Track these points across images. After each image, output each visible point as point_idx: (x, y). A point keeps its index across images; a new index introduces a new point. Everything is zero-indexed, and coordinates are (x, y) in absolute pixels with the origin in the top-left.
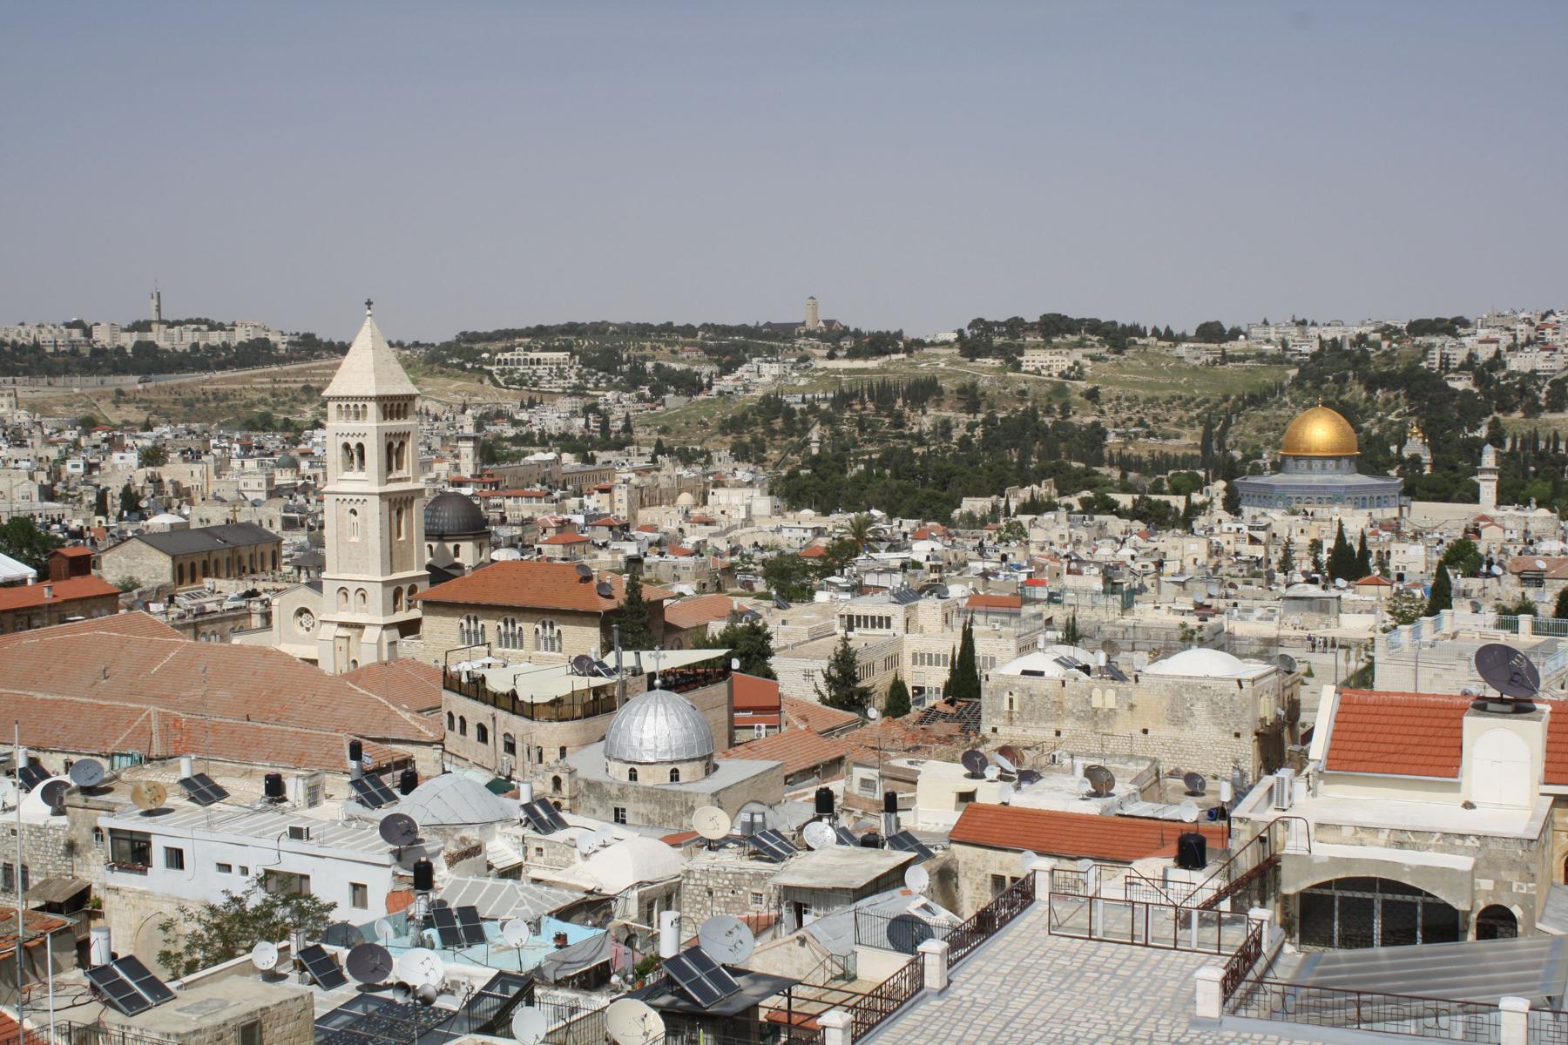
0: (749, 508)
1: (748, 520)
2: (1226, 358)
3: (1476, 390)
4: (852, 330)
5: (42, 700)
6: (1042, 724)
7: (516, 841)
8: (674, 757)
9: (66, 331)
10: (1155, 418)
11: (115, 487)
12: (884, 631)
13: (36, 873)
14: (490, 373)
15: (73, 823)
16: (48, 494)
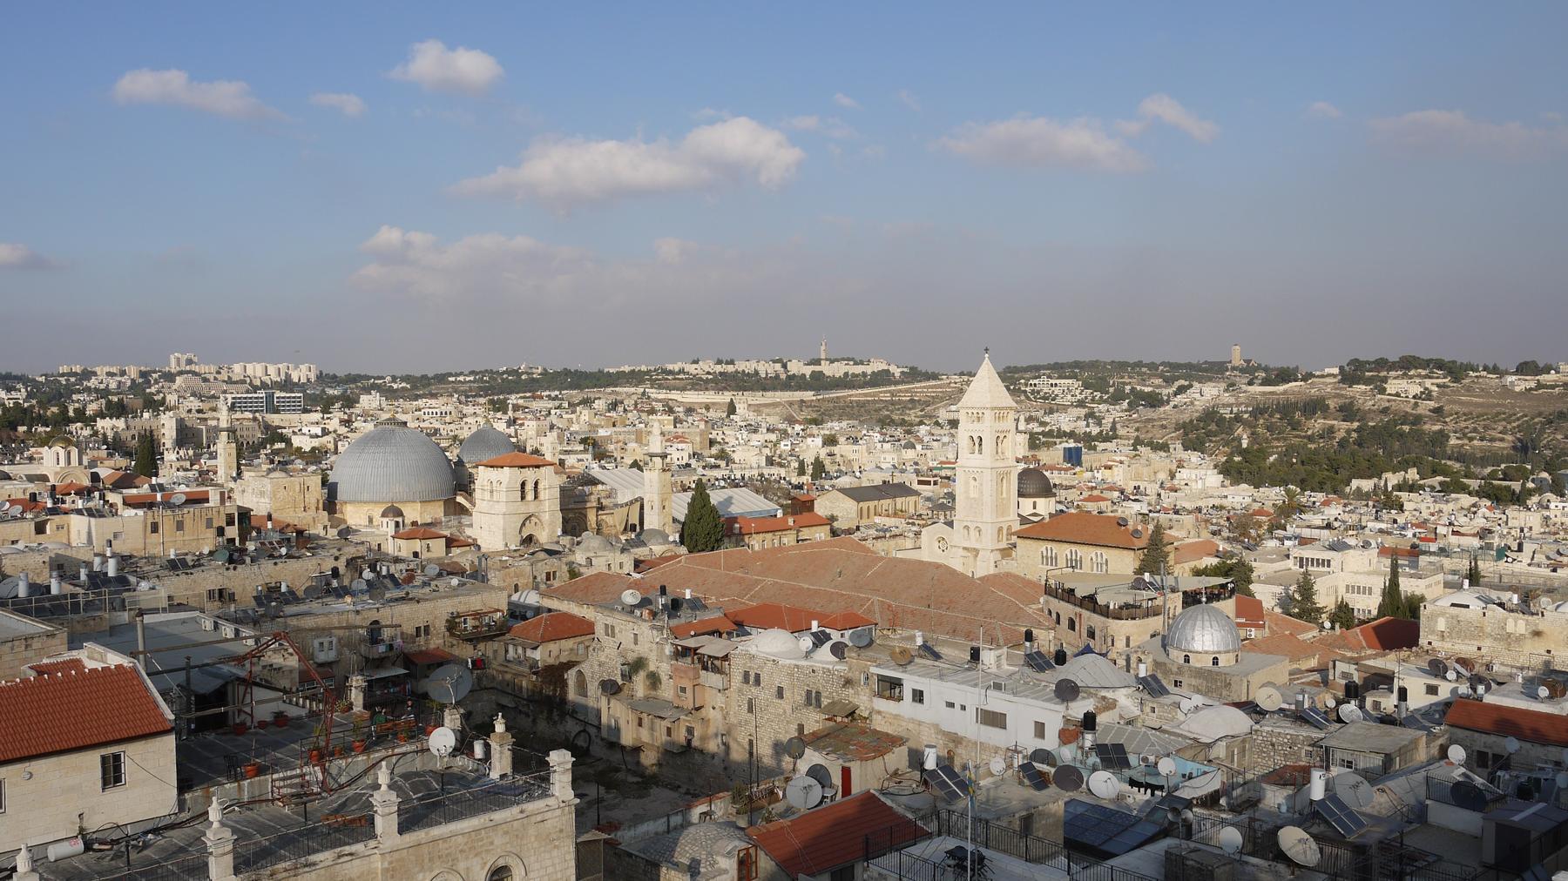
2: (1540, 386)
5: (808, 588)
6: (1467, 641)
7: (1136, 701)
8: (1216, 649)
9: (772, 365)
10: (1485, 427)
11: (809, 459)
13: (827, 697)
14: (1025, 392)
15: (850, 669)
16: (770, 462)
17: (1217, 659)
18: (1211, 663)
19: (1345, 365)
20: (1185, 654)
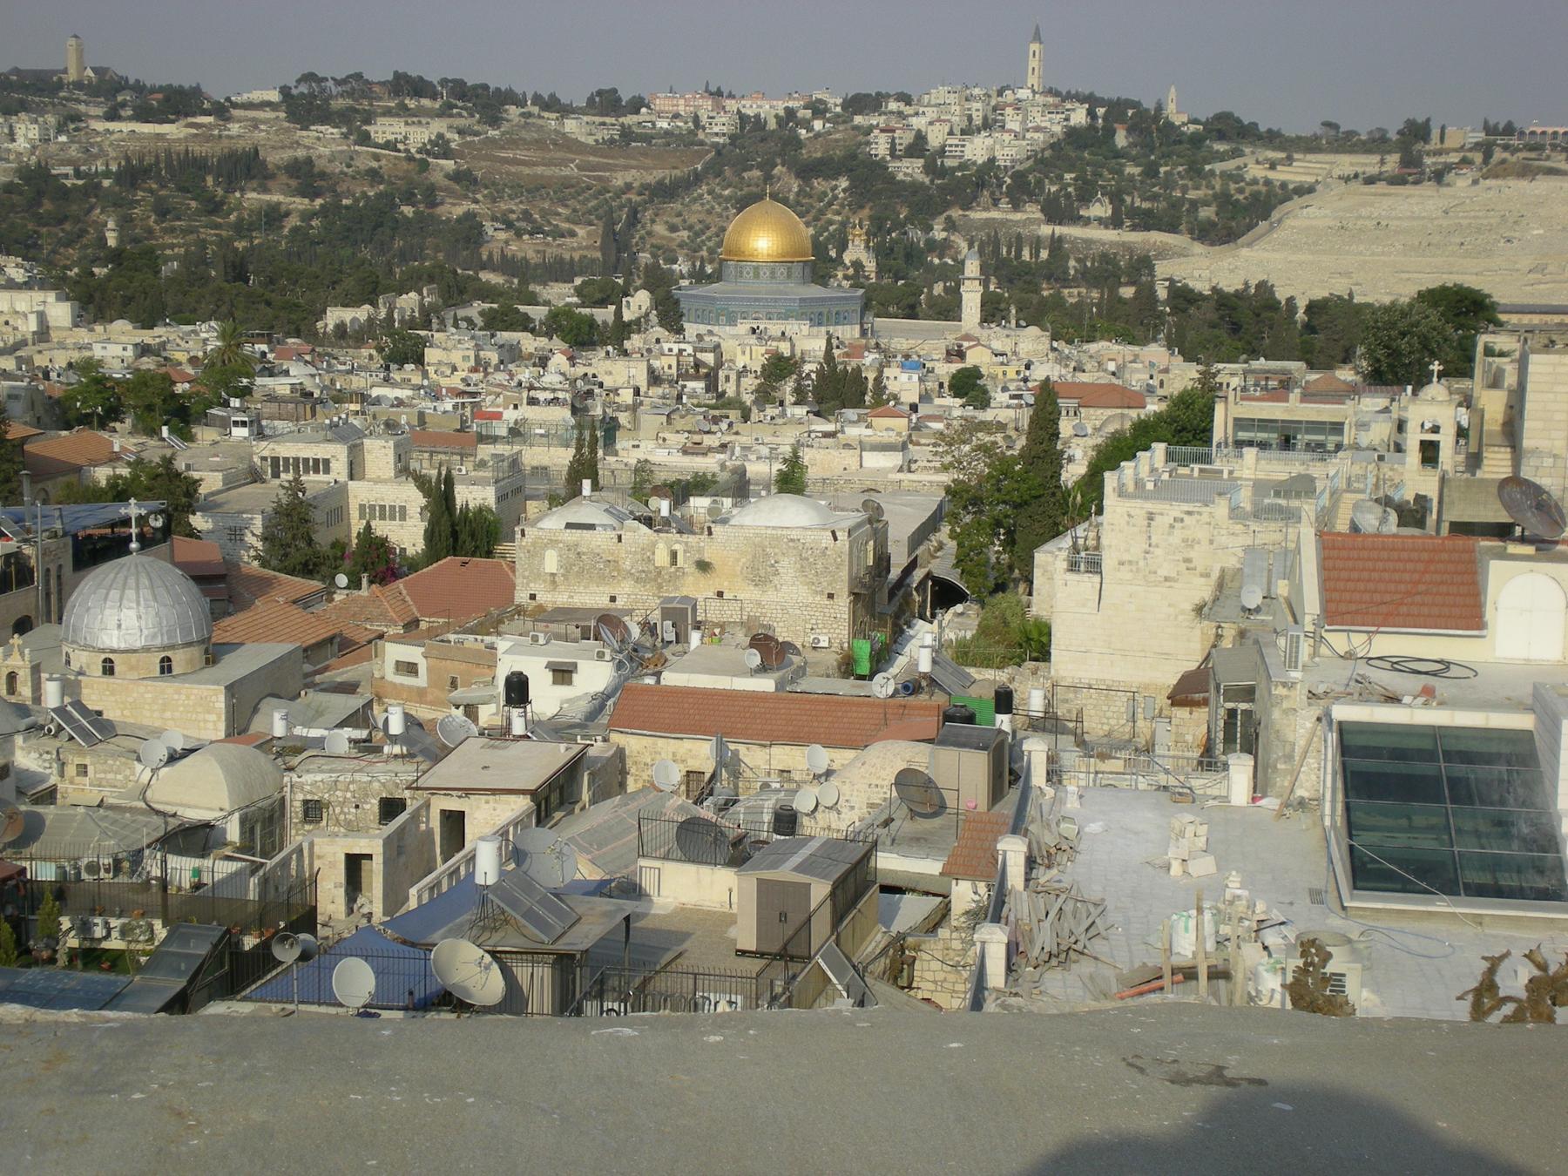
0: (41, 317)
1: (43, 333)
3: (364, 128)
4: (131, 81)
6: (593, 588)
8: (166, 641)
10: (544, 213)
12: (321, 477)
17: (169, 660)
18: (158, 669)
19: (292, 84)
20: (104, 656)
